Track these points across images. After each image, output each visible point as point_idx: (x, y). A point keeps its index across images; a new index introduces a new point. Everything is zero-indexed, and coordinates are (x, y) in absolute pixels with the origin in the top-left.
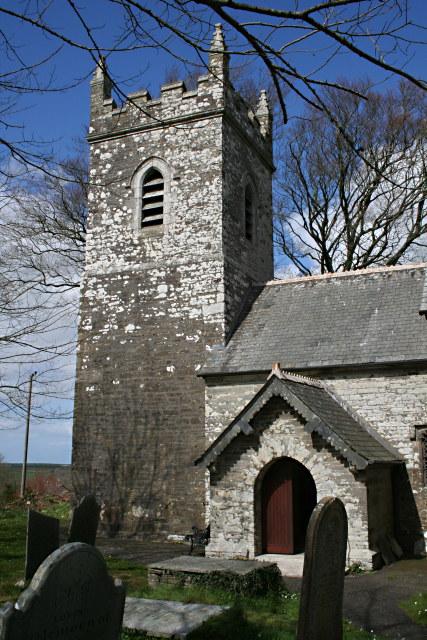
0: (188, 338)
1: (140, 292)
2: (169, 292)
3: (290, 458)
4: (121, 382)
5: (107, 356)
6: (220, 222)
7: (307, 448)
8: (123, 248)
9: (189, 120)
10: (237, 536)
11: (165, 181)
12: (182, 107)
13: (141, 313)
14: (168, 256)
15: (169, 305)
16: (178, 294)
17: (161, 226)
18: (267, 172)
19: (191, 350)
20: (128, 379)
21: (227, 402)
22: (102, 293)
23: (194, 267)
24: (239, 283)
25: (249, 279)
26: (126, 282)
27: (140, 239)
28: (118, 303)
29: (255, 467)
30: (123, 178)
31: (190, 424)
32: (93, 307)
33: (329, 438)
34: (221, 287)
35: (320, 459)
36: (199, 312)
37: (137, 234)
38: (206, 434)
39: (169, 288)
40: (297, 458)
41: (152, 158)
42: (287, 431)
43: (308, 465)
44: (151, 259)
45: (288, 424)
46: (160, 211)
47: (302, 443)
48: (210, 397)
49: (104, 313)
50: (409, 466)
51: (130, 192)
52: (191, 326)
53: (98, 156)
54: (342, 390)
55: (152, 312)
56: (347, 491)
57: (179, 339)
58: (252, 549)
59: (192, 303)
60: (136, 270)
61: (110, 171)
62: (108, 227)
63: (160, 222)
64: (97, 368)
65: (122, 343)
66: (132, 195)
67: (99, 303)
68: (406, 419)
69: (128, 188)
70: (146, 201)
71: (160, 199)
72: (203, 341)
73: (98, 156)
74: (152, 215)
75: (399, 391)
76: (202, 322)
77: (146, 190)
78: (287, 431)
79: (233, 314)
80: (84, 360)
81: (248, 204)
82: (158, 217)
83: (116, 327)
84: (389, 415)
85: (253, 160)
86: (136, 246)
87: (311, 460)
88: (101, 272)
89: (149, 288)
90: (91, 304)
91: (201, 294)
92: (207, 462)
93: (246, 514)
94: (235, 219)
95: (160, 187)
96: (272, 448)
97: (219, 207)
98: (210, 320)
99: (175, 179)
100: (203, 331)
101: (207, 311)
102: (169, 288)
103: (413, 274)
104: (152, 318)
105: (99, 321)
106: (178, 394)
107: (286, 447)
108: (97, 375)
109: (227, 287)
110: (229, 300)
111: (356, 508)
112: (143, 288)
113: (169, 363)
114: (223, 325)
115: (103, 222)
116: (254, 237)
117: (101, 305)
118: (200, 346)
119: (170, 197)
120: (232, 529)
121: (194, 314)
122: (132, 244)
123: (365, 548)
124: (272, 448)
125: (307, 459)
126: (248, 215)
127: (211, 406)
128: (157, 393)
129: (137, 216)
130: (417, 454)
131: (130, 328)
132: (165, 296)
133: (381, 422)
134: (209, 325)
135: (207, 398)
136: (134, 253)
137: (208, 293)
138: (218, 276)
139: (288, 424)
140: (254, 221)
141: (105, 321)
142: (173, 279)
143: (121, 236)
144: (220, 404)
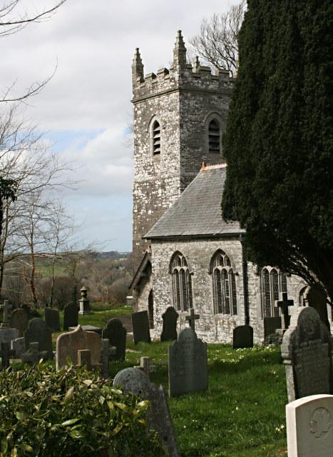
12: (165, 85)
66: (149, 136)
92: (133, 287)
122: (150, 165)
129: (151, 149)
131: (150, 212)
142: (163, 187)
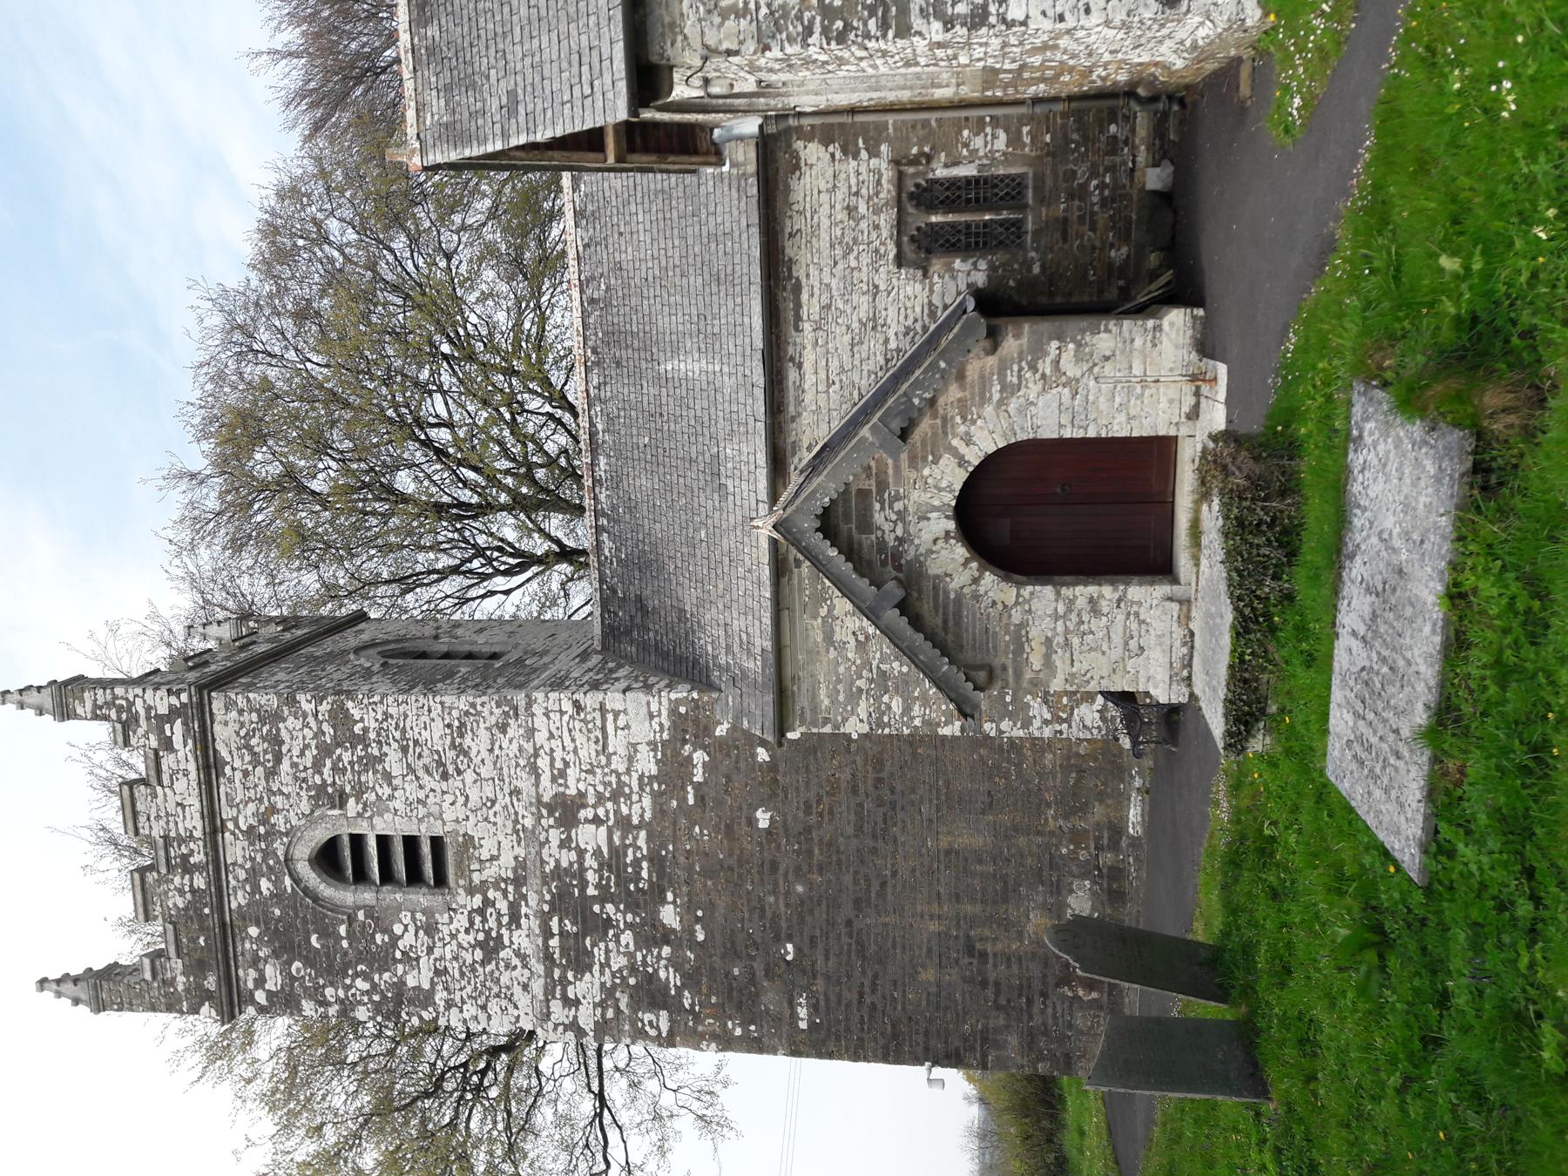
0: (698, 778)
1: (591, 891)
2: (597, 821)
3: (960, 499)
4: (790, 939)
5: (728, 974)
6: (448, 700)
7: (935, 462)
8: (488, 933)
9: (210, 766)
10: (1134, 626)
11: (345, 831)
13: (638, 889)
14: (516, 822)
15: (624, 823)
16: (600, 799)
17: (447, 840)
18: (362, 626)
19: (723, 769)
20: (784, 924)
21: (839, 681)
22: (587, 987)
23: (543, 762)
24: (590, 670)
25: (584, 656)
26: (569, 926)
27: (471, 891)
28: (611, 945)
29: (976, 581)
30: (327, 933)
31: (885, 775)
32: (618, 1011)
33: (916, 401)
34: (590, 700)
35: (962, 429)
36: (643, 748)
37: (462, 897)
38: (906, 731)
39: (587, 821)
40: (958, 487)
41: (288, 860)
42: (898, 506)
43: (974, 457)
44: (520, 864)
45: (882, 503)
46: (411, 843)
47: (926, 472)
48: (826, 721)
49: (632, 981)
50: (980, 279)
51: (361, 915)
52: (673, 770)
53: (270, 994)
54: (813, 426)
55: (637, 863)
56: (1033, 368)
57: (701, 799)
58: (1162, 590)
59: (622, 768)
60: (542, 900)
61: (308, 962)
62: (437, 972)
63: (437, 843)
64: (755, 998)
65: (701, 937)
67: (609, 992)
68: (882, 287)
69: (351, 919)
70: (387, 876)
71: (384, 842)
72: (707, 741)
73: (270, 994)
74: (421, 863)
75: (825, 300)
76: (664, 743)
77: (361, 876)
78: (898, 506)
79: (652, 680)
80: (738, 1032)
81: (423, 655)
82: (426, 849)
83: (666, 951)
84: (874, 323)
85: (329, 645)
86: (487, 902)
87: (963, 449)
88: (538, 986)
89: (583, 870)
90: (610, 1014)
91: (605, 747)
93: (1081, 602)
94: (450, 675)
95: (357, 841)
96: (935, 541)
97: (416, 700)
98: (661, 725)
99: (342, 806)
100: (685, 742)
101: (643, 731)
102: (587, 821)
103: (592, 301)
104: (651, 860)
105: (650, 994)
106: (819, 802)
107: (935, 509)
108: (770, 1000)
109: (595, 686)
110: (623, 684)
111: (1071, 346)
112: (584, 884)
113: (752, 822)
114: (673, 696)
115: (426, 986)
116: (497, 649)
117: (614, 986)
118: (719, 749)
119: (394, 816)
120: (1117, 638)
121: (647, 764)
122: (481, 911)
123: (1160, 326)
124: (935, 541)
125: (962, 462)
126: (447, 656)
127: (845, 720)
128: (816, 851)
130: (958, 264)
131: (669, 916)
132: (603, 829)
133: (887, 341)
134: (674, 726)
135: (827, 729)
136: (503, 906)
137: (604, 729)
138: (567, 706)
139: (882, 503)
140: (467, 648)
141: (652, 978)
142: (566, 811)
143: (462, 936)
144: (841, 698)
